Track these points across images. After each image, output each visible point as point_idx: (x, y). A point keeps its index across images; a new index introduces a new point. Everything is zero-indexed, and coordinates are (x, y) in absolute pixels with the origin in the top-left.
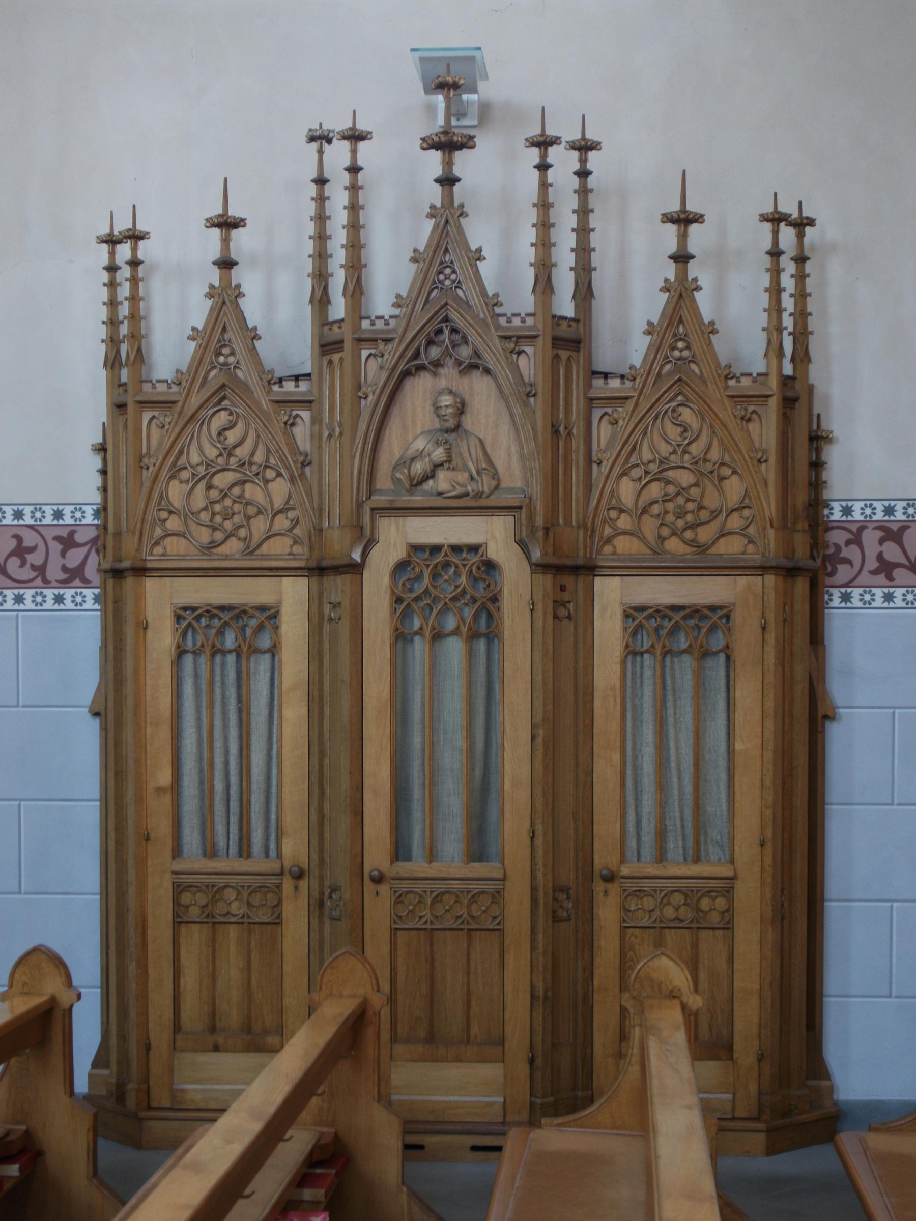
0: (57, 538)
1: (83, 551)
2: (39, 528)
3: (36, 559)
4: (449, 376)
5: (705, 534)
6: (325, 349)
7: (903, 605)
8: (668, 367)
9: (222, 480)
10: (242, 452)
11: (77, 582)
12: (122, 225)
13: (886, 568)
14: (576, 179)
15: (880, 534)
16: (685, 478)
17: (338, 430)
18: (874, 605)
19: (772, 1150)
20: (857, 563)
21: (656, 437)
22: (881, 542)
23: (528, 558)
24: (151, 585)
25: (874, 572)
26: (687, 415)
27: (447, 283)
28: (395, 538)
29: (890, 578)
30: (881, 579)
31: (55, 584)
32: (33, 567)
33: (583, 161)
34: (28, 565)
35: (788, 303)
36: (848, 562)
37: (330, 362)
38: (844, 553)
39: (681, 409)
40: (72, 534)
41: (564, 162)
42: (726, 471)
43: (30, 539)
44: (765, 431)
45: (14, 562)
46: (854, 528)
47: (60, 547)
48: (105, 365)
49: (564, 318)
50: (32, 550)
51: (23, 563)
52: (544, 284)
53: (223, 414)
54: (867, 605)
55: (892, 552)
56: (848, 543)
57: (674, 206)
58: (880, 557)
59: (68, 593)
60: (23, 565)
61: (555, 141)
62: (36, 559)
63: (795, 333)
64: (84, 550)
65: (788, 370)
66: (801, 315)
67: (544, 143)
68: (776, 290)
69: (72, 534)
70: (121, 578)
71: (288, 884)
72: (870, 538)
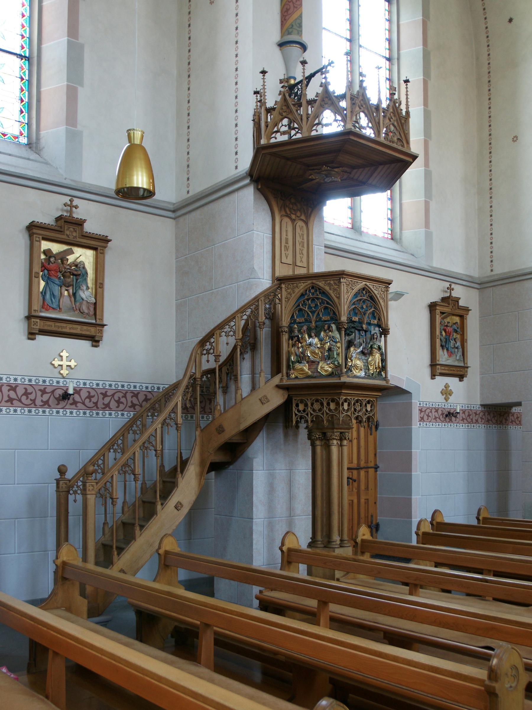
0: (40, 390)
1: (109, 398)
2: (34, 386)
3: (32, 397)
6: (92, 331)
7: (20, 413)
11: (46, 406)
13: (10, 400)
15: (9, 388)
18: (39, 414)
19: (436, 567)
20: (125, 403)
22: (9, 390)
25: (6, 401)
29: (12, 404)
31: (100, 409)
32: (31, 400)
34: (29, 399)
40: (106, 392)
43: (93, 393)
45: (87, 401)
46: (124, 392)
47: (41, 393)
50: (93, 396)
51: (27, 398)
54: (37, 414)
55: (12, 394)
56: (123, 397)
60: (90, 401)
62: (32, 397)
69: (106, 392)
70: (501, 423)
72: (129, 395)
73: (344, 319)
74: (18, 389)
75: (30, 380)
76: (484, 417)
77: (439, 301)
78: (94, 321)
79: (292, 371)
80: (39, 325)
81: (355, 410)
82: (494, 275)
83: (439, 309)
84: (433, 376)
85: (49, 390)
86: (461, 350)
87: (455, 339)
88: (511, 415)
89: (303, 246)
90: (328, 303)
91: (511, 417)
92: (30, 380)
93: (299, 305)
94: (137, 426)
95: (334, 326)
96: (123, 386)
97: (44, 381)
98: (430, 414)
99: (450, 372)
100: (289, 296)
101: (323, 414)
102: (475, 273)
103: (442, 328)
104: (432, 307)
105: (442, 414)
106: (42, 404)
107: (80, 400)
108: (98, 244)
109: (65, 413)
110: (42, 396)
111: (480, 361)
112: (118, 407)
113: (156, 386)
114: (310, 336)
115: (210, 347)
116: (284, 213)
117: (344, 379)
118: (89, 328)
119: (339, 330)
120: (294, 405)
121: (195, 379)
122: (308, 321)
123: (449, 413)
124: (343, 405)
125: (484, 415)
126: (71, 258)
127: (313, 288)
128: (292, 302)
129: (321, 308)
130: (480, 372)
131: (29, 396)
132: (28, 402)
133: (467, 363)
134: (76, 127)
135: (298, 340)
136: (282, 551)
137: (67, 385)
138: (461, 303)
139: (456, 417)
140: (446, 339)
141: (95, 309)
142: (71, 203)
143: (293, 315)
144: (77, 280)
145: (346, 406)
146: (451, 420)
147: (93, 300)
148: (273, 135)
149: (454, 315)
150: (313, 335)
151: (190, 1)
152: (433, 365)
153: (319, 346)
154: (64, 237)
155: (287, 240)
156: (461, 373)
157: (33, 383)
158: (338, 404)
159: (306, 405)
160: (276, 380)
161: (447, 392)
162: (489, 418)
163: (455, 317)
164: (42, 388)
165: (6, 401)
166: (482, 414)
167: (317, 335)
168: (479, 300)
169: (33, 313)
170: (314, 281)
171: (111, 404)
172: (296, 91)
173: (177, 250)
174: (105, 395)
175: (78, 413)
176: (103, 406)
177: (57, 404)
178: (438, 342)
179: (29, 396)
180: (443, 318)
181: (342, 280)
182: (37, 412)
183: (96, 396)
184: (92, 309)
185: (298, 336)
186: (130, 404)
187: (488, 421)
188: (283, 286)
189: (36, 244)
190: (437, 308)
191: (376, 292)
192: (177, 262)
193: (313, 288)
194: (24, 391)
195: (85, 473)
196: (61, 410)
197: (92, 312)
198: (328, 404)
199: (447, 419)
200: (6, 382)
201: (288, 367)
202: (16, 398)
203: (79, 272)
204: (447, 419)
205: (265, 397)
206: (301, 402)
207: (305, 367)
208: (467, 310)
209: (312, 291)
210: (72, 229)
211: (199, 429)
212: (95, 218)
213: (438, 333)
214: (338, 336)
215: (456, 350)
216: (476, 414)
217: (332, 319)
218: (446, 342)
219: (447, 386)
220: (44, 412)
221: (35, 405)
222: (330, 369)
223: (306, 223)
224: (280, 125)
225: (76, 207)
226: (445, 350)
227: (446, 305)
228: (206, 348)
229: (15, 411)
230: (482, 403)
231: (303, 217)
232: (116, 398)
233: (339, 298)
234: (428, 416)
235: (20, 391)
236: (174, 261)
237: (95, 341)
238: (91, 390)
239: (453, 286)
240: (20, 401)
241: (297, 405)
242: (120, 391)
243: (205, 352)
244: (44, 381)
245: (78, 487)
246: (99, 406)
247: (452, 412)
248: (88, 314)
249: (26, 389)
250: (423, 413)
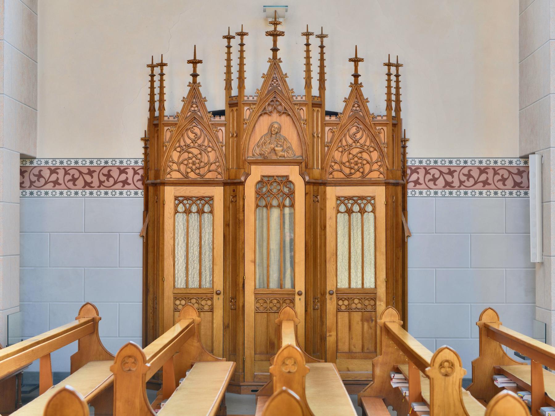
0: (420, 184)
4: (275, 117)
5: (202, 171)
8: (190, 113)
9: (355, 151)
10: (362, 141)
12: (157, 61)
14: (305, 47)
16: (195, 151)
17: (235, 135)
18: (101, 196)
21: (348, 136)
22: (92, 182)
23: (304, 179)
24: (329, 189)
26: (197, 130)
27: (275, 85)
28: (257, 173)
29: (449, 169)
30: (92, 169)
31: (491, 168)
33: (229, 42)
35: (393, 91)
37: (232, 110)
38: (36, 178)
39: (194, 128)
41: (315, 42)
42: (209, 149)
44: (384, 135)
49: (315, 97)
51: (433, 175)
52: (308, 85)
53: (355, 128)
57: (353, 56)
59: (58, 164)
61: (312, 34)
63: (394, 100)
64: (50, 180)
65: (393, 114)
66: (398, 95)
67: (307, 34)
68: (389, 87)
71: (215, 297)
74: (512, 184)
106: (126, 170)
107: (514, 176)
109: (443, 162)
110: (127, 178)
112: (40, 171)
131: (432, 178)
137: (22, 191)
151: (21, 386)
165: (94, 171)
171: (48, 175)
174: (485, 183)
175: (473, 162)
176: (58, 171)
179: (432, 178)
182: (443, 162)
183: (427, 180)
194: (506, 183)
200: (27, 191)
202: (445, 175)
221: (64, 169)
232: (112, 181)
235: (80, 182)
238: (434, 187)
240: (81, 173)
242: (109, 187)
246: (493, 171)
249: (504, 185)
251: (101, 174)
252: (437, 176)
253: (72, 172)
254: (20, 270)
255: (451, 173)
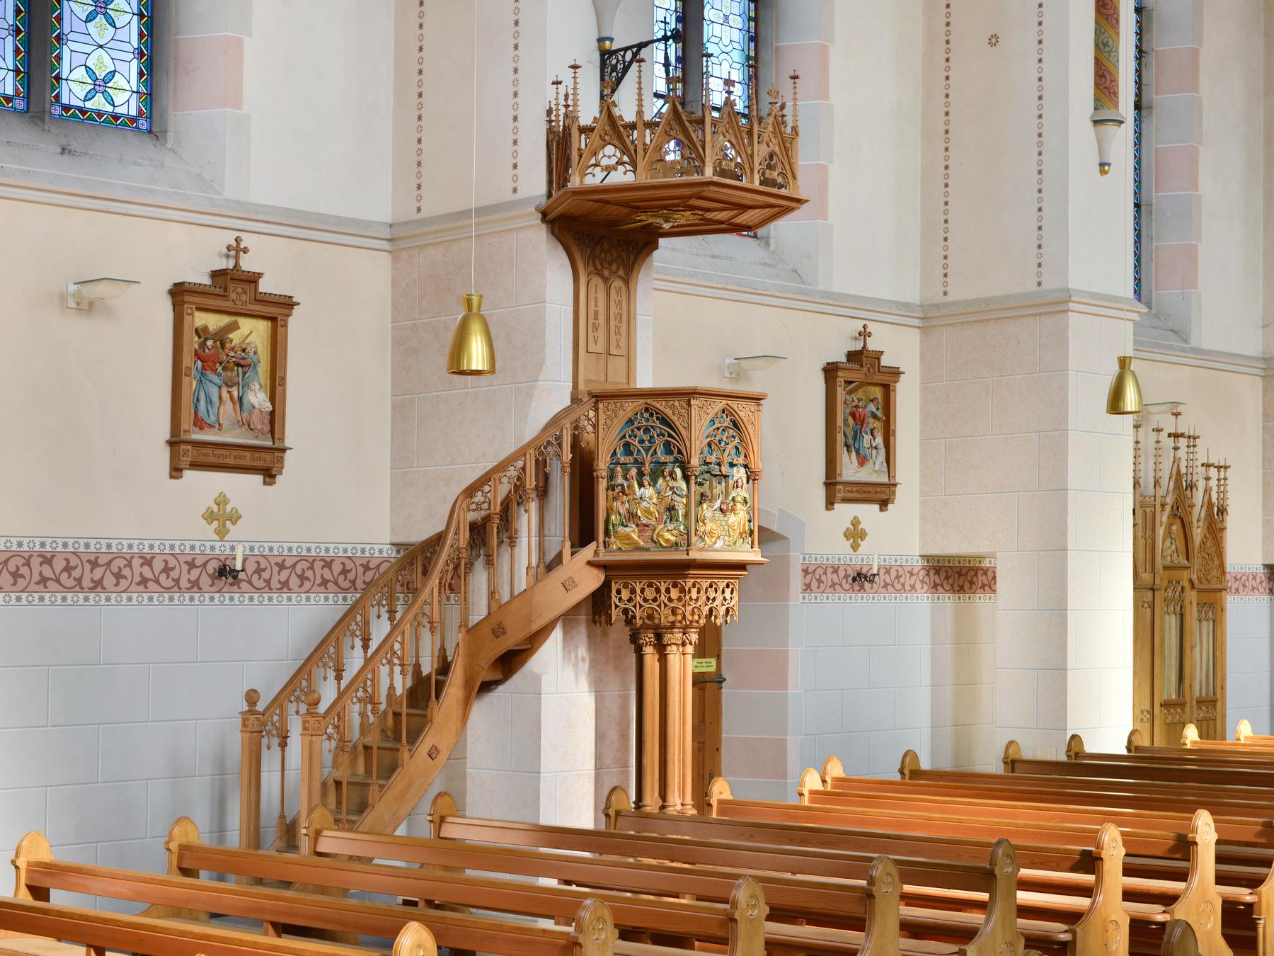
11: (195, 589)
20: (312, 578)
22: (41, 564)
25: (37, 583)
29: (45, 587)
30: (41, 587)
36: (23, 577)
46: (311, 560)
48: (175, 285)
55: (147, 572)
58: (141, 574)
59: (92, 595)
62: (77, 573)
70: (961, 589)
72: (35, 562)
73: (695, 461)
75: (172, 547)
76: (927, 579)
77: (844, 359)
78: (270, 443)
79: (613, 539)
80: (188, 453)
81: (708, 598)
82: (949, 304)
83: (842, 377)
84: (830, 504)
85: (199, 562)
86: (883, 451)
87: (872, 431)
88: (980, 572)
89: (620, 321)
90: (670, 436)
91: (980, 577)
92: (172, 547)
93: (624, 437)
94: (357, 624)
95: (678, 472)
96: (309, 550)
97: (193, 547)
98: (823, 578)
99: (864, 496)
100: (609, 422)
101: (659, 606)
102: (912, 294)
103: (848, 411)
104: (830, 371)
105: (846, 577)
108: (277, 311)
111: (921, 471)
113: (359, 547)
114: (641, 485)
115: (482, 499)
116: (591, 268)
117: (694, 555)
118: (264, 455)
119: (686, 478)
120: (614, 592)
121: (458, 548)
122: (639, 464)
123: (859, 574)
124: (690, 592)
125: (928, 575)
126: (235, 337)
127: (647, 410)
128: (614, 433)
129: (660, 442)
130: (921, 491)
132: (169, 583)
133: (894, 477)
134: (240, 108)
135: (623, 492)
136: (607, 815)
138: (885, 361)
139: (872, 581)
140: (856, 433)
141: (272, 422)
142: (238, 244)
143: (615, 453)
144: (244, 373)
145: (694, 594)
146: (862, 587)
147: (268, 406)
148: (590, 170)
149: (870, 384)
150: (646, 483)
152: (831, 484)
153: (655, 500)
154: (230, 304)
155: (596, 313)
156: (884, 497)
157: (177, 551)
158: (682, 590)
159: (633, 591)
160: (588, 552)
161: (855, 534)
162: (938, 581)
163: (872, 389)
164: (189, 559)
166: (922, 573)
167: (654, 482)
168: (921, 348)
169: (184, 437)
170: (649, 401)
172: (614, 62)
173: (395, 309)
177: (212, 585)
178: (840, 438)
180: (850, 393)
181: (693, 402)
184: (267, 421)
185: (622, 485)
186: (319, 580)
187: (935, 586)
188: (601, 405)
189: (187, 319)
190: (840, 374)
191: (742, 414)
192: (393, 328)
193: (647, 410)
195: (278, 702)
196: (217, 595)
197: (267, 428)
198: (668, 591)
199: (856, 587)
201: (607, 533)
203: (249, 361)
204: (856, 587)
205: (571, 579)
206: (626, 587)
207: (632, 531)
208: (896, 373)
209: (646, 415)
210: (240, 290)
211: (463, 630)
212: (274, 267)
213: (840, 422)
214: (684, 486)
215: (874, 452)
216: (911, 574)
217: (676, 460)
218: (855, 438)
219: (856, 522)
220: (192, 599)
221: (82, 588)
222: (673, 538)
223: (627, 281)
224: (601, 155)
225: (245, 251)
226: (854, 454)
227: (857, 367)
228: (476, 500)
229: (150, 599)
230: (924, 553)
231: (621, 273)
233: (689, 428)
234: (819, 581)
236: (390, 326)
237: (269, 475)
239: (871, 327)
241: (619, 592)
242: (304, 559)
243: (473, 506)
244: (193, 547)
245: (273, 724)
247: (864, 571)
248: (262, 432)
249: (166, 562)
250: (809, 577)
251: (28, 578)
252: (65, 575)
253: (71, 583)
254: (1187, 858)
255: (43, 580)
